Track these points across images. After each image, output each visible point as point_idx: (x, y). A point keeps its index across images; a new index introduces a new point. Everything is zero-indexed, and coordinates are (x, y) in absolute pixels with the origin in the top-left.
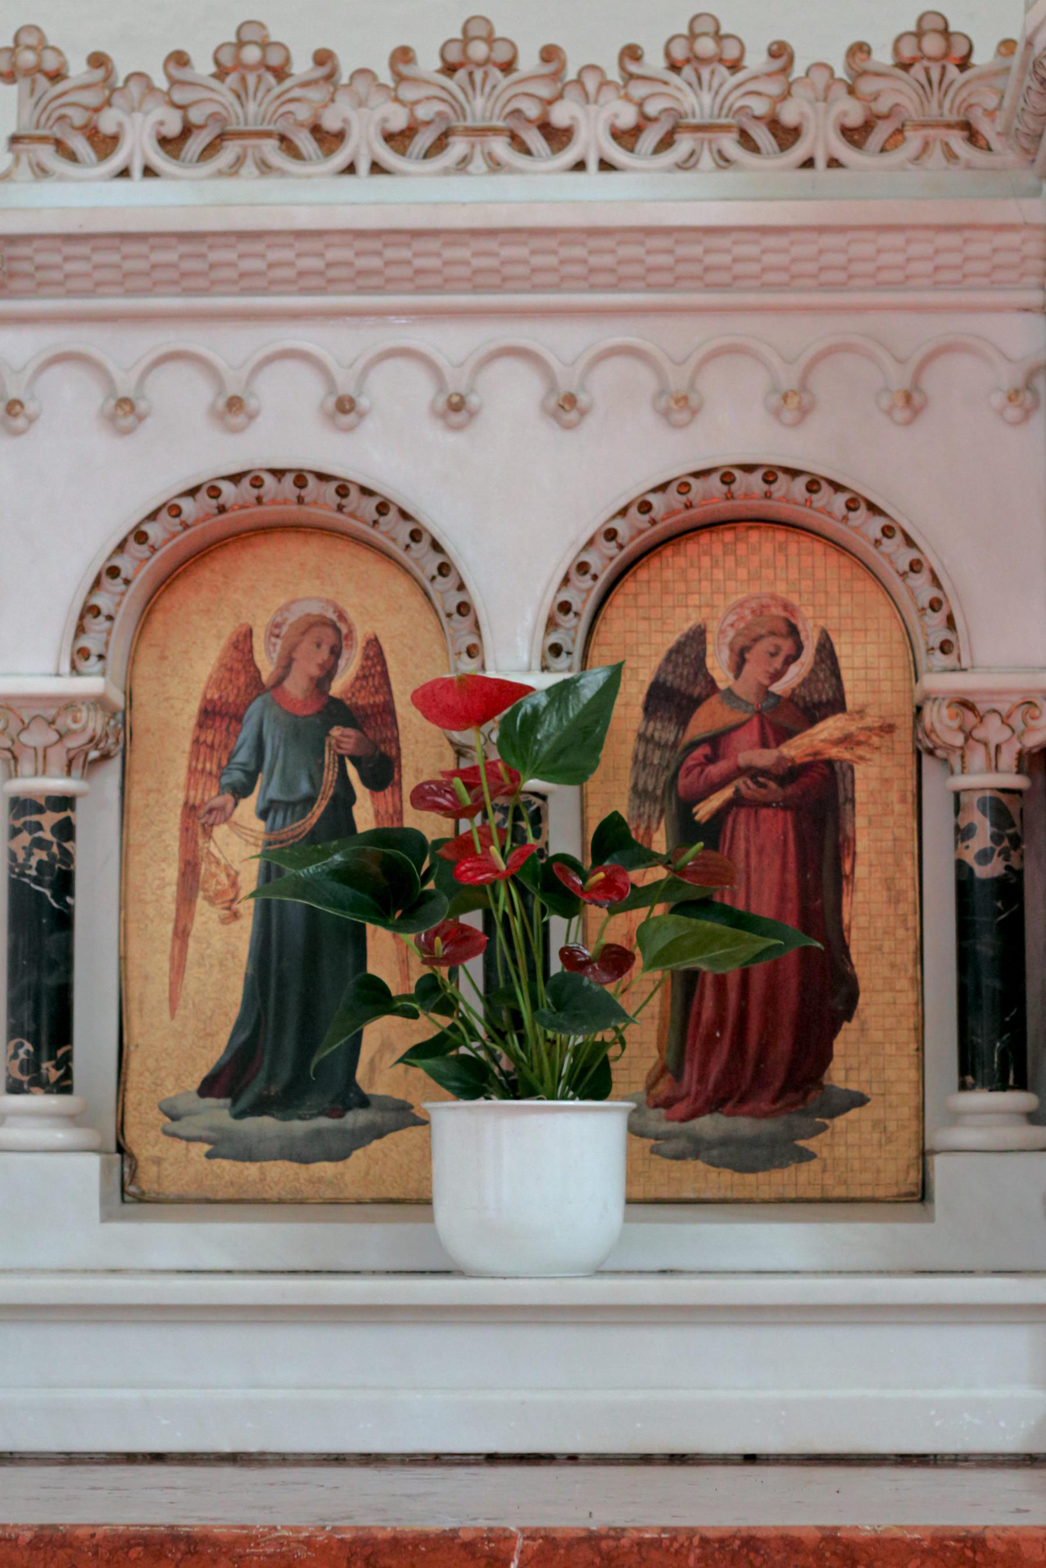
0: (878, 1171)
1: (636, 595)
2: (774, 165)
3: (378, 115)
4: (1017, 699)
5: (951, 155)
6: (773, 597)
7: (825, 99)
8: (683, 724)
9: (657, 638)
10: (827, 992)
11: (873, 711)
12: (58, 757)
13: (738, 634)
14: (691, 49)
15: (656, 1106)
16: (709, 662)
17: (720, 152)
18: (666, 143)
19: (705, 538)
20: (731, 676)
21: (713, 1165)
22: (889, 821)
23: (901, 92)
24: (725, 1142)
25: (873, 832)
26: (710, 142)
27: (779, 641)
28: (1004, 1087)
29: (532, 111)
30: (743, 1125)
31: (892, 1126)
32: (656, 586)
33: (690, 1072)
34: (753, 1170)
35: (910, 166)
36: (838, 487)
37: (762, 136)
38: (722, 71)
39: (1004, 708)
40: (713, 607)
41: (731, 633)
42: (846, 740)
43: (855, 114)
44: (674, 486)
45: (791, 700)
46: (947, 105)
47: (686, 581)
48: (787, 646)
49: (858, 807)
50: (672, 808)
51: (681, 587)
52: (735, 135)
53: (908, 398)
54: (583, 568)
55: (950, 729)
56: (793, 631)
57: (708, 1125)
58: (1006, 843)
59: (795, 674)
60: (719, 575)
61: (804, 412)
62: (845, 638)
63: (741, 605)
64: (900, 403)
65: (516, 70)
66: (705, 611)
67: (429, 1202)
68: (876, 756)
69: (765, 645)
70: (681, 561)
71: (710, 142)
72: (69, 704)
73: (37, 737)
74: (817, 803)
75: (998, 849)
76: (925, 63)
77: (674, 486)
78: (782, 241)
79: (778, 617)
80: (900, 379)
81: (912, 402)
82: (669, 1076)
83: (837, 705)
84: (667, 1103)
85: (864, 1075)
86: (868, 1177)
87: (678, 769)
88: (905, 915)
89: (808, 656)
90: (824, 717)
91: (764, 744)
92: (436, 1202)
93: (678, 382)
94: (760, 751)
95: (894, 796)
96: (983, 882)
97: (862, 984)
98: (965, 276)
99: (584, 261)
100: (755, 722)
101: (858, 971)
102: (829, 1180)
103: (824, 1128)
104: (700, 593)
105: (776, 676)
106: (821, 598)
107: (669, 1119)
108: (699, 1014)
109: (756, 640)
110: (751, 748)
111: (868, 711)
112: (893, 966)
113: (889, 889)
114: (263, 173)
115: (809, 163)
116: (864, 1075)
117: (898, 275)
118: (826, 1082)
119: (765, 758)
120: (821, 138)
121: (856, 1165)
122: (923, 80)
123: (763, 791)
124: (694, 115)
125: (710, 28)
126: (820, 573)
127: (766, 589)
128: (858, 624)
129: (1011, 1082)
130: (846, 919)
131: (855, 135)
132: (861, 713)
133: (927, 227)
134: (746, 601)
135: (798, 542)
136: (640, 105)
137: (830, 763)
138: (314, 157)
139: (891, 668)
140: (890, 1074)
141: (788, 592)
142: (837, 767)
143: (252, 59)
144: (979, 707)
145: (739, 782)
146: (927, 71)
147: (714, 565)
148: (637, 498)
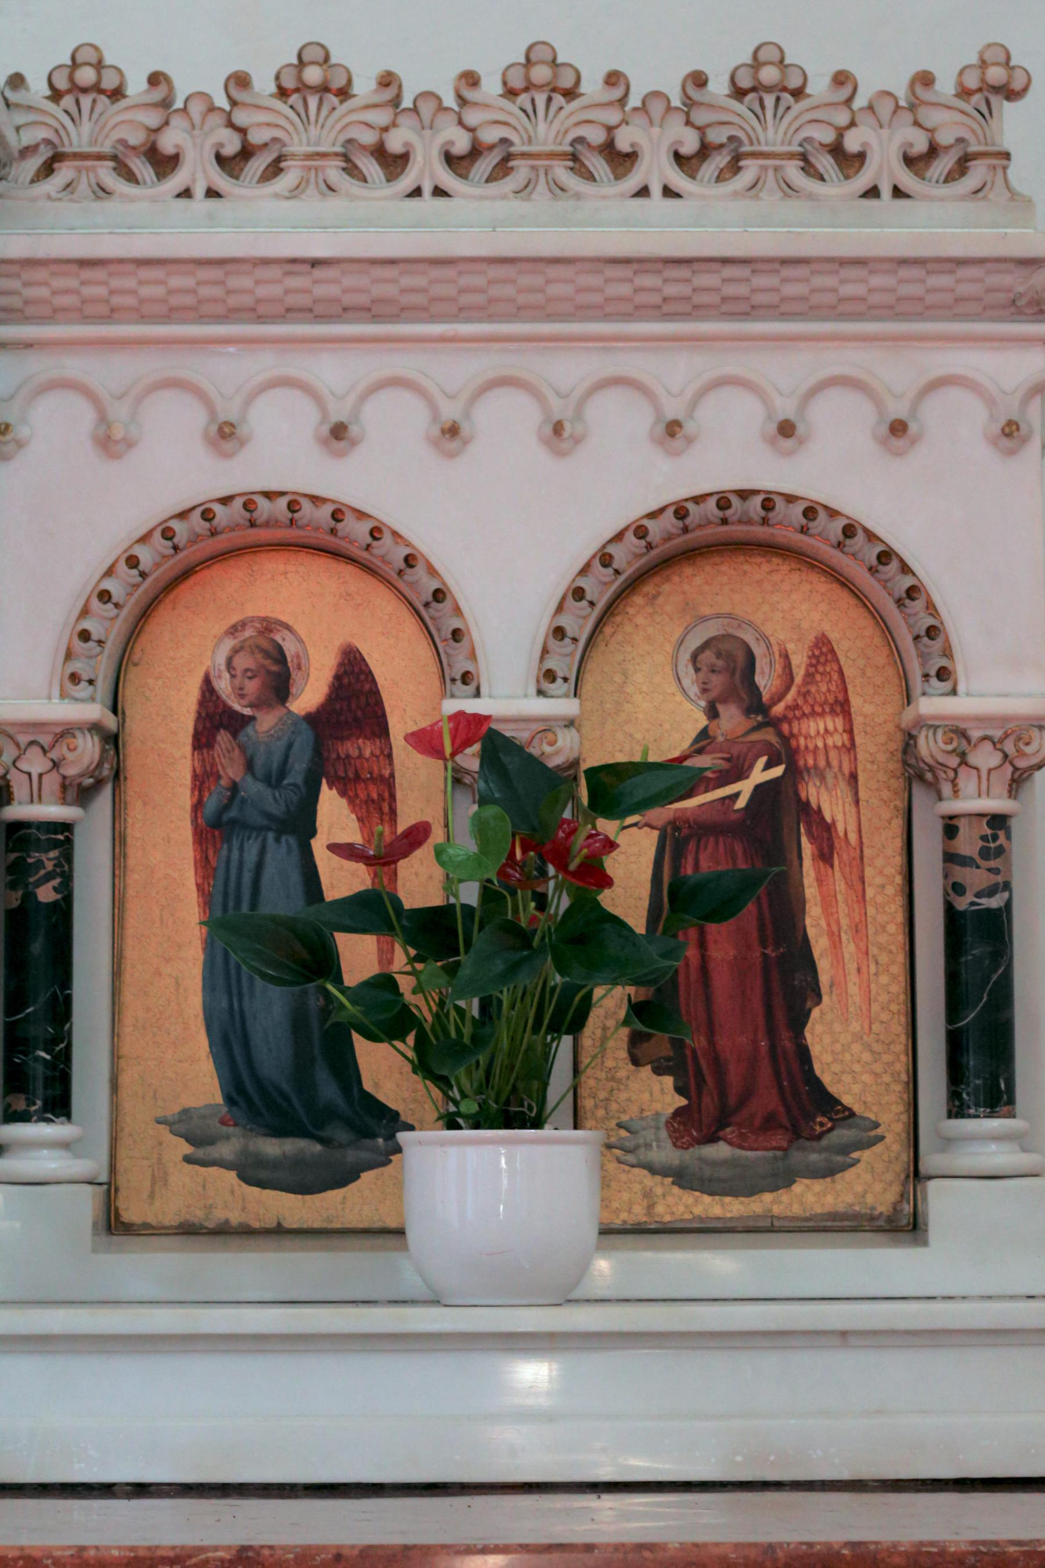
2: (838, 189)
3: (212, 140)
12: (52, 783)
29: (368, 138)
54: (578, 593)
65: (124, 96)
67: (400, 1232)
72: (66, 732)
73: (35, 763)
92: (407, 1231)
99: (77, 292)
114: (786, 195)
138: (149, 182)
143: (770, 82)
148: (634, 522)
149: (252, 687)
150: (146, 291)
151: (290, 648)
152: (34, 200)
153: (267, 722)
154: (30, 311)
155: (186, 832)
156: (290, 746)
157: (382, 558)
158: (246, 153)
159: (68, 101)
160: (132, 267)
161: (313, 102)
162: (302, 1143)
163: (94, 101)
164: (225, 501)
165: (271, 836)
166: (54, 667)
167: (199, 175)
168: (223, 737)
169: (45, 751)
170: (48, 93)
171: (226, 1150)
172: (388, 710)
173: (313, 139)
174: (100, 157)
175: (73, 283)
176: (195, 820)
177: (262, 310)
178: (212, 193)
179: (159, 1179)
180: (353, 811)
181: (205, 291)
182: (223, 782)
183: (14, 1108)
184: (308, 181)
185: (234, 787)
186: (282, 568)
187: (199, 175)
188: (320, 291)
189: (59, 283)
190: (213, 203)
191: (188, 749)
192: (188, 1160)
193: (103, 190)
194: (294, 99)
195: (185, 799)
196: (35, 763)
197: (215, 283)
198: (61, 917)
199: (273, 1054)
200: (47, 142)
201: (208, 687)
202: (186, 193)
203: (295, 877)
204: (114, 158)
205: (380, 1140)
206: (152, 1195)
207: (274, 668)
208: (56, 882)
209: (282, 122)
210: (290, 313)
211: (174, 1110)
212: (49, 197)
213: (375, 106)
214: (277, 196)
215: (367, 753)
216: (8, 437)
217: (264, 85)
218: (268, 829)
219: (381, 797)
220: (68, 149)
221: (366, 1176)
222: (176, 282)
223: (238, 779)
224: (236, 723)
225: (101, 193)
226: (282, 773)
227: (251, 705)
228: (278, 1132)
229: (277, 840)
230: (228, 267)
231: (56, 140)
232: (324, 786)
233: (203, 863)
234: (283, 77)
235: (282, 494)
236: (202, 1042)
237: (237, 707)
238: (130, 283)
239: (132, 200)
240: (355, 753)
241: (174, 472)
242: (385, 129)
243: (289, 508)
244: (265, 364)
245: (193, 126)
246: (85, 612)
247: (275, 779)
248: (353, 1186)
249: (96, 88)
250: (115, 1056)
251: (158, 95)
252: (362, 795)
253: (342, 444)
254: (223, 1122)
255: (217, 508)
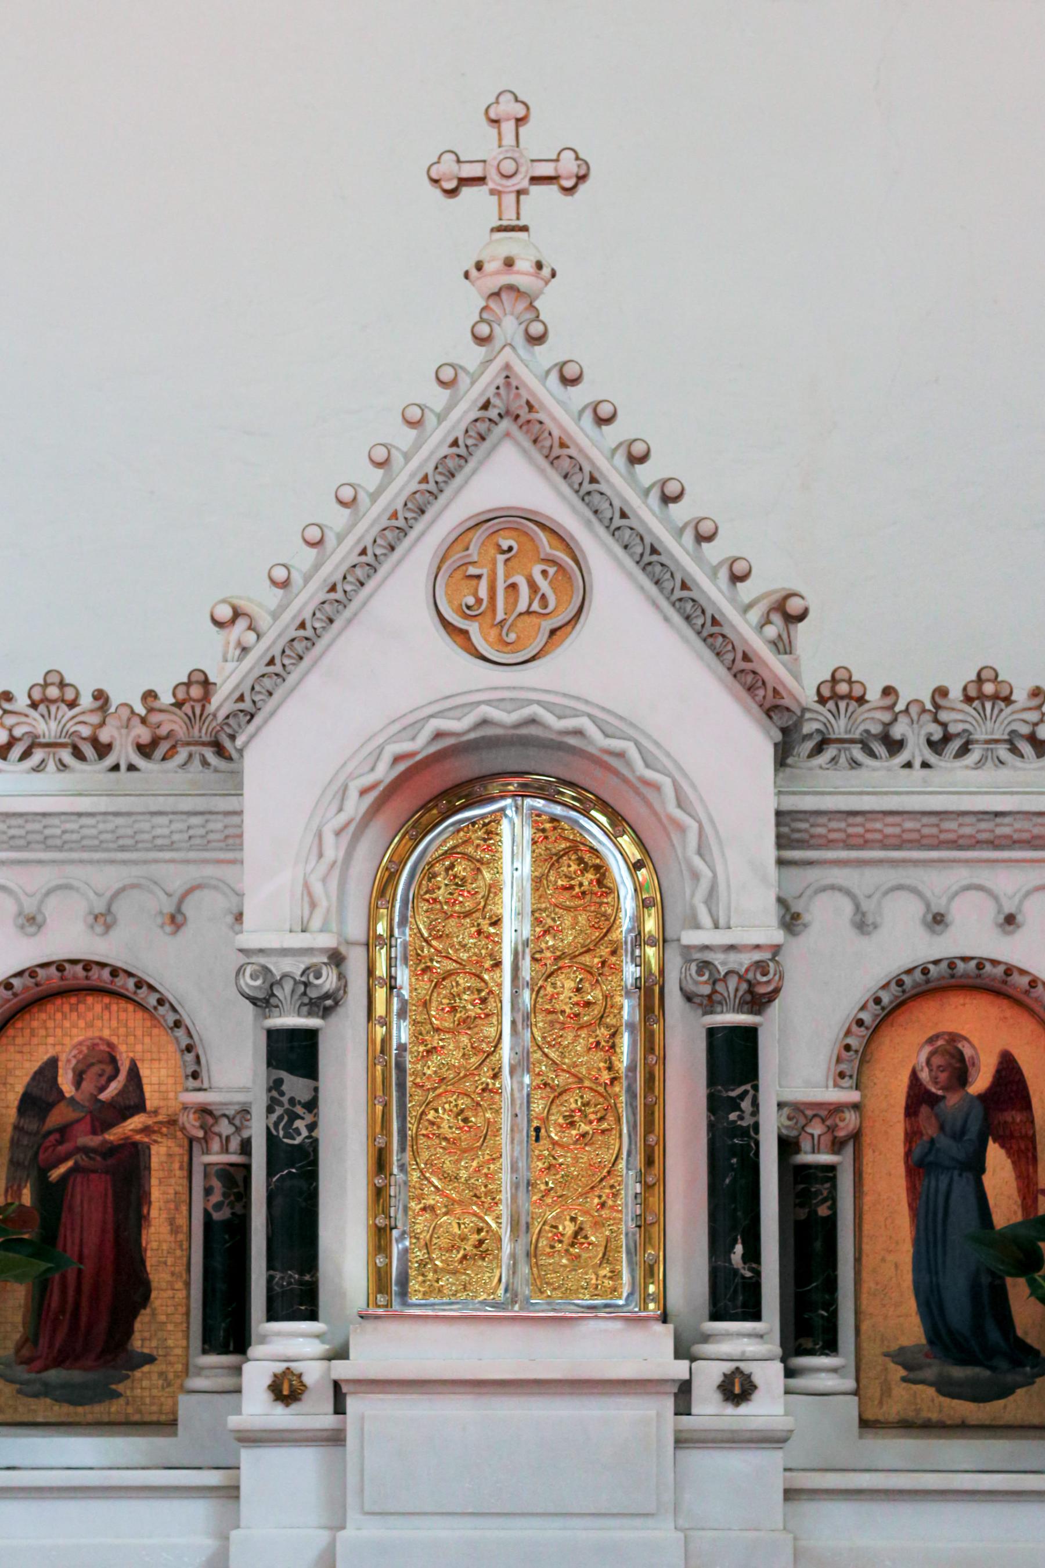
0: (162, 1405)
1: (14, 1037)
4: (237, 1107)
5: (205, 763)
6: (101, 1038)
7: (127, 727)
8: (43, 1120)
9: (27, 1065)
10: (130, 1288)
11: (163, 1111)
12: (826, 1140)
13: (78, 1062)
14: (44, 693)
15: (22, 1363)
16: (60, 1080)
17: (60, 760)
18: (26, 755)
19: (58, 1001)
20: (73, 1089)
21: (56, 1400)
22: (173, 1181)
23: (175, 722)
24: (64, 1386)
25: (162, 1190)
26: (54, 754)
27: (103, 1066)
28: (226, 1352)
29: (1025, 730)
30: (76, 1376)
31: (171, 1376)
32: (27, 1032)
33: (43, 1341)
34: (81, 1404)
35: (180, 770)
36: (130, 974)
37: (88, 750)
38: (64, 707)
39: (231, 1112)
40: (63, 1045)
41: (74, 1062)
42: (146, 1130)
43: (144, 735)
44: (27, 974)
45: (111, 1104)
46: (204, 731)
47: (46, 1029)
48: (109, 1070)
49: (153, 1173)
50: (34, 1173)
51: (42, 1032)
52: (70, 750)
53: (173, 918)
55: (193, 1126)
56: (113, 1060)
57: (53, 1375)
58: (232, 1198)
59: (114, 1087)
60: (67, 1024)
61: (108, 927)
62: (146, 1065)
63: (80, 1044)
64: (168, 920)
66: (58, 1048)
67: (239, 1468)
68: (164, 1140)
69: (95, 1069)
70: (43, 1016)
71: (54, 754)
72: (837, 1109)
74: (128, 1168)
75: (227, 1202)
76: (192, 703)
77: (27, 974)
78: (90, 821)
79: (103, 1051)
80: (169, 907)
81: (176, 921)
82: (29, 1344)
83: (140, 1107)
84: (27, 1361)
85: (154, 1344)
86: (154, 1408)
87: (39, 1148)
88: (181, 1241)
89: (122, 1077)
90: (132, 1115)
91: (94, 1132)
93: (30, 906)
94: (91, 1137)
95: (177, 1165)
96: (217, 1222)
97: (154, 1285)
98: (209, 842)
100: (88, 1117)
101: (151, 1277)
102: (130, 1410)
103: (127, 1377)
104: (55, 1036)
105: (102, 1089)
106: (131, 1039)
107: (30, 1371)
108: (49, 1305)
109: (91, 1065)
110: (86, 1135)
111: (160, 1111)
112: (173, 1274)
113: (171, 1224)
115: (116, 768)
116: (154, 1344)
117: (167, 842)
118: (129, 1348)
119: (93, 1141)
120: (124, 752)
121: (148, 1400)
122: (190, 714)
123: (92, 1162)
124: (44, 736)
125: (57, 680)
126: (131, 1024)
127: (97, 1034)
128: (155, 1056)
129: (231, 1348)
130: (144, 1245)
131: (145, 750)
132: (156, 1112)
133: (182, 813)
134: (84, 1041)
135: (118, 1003)
136: (10, 730)
137: (135, 1145)
139: (175, 1084)
140: (170, 1343)
141: (111, 1035)
142: (140, 1146)
144: (215, 1112)
145: (78, 1157)
146: (193, 708)
147: (64, 1017)
149: (943, 1076)
150: (889, 830)
151: (968, 1052)
152: (811, 769)
153: (953, 1100)
154: (812, 842)
155: (901, 1170)
156: (968, 1115)
157: (1036, 999)
158: (947, 738)
159: (831, 705)
160: (880, 816)
161: (988, 705)
162: (977, 1370)
163: (848, 705)
164: (936, 962)
165: (956, 1173)
166: (829, 1068)
167: (917, 753)
168: (924, 1110)
169: (823, 1121)
170: (816, 699)
171: (930, 1373)
172: (1031, 1093)
173: (989, 730)
174: (852, 741)
175: (842, 825)
176: (906, 1162)
177: (961, 842)
178: (925, 765)
179: (886, 1391)
180: (1009, 1157)
181: (926, 831)
182: (925, 1138)
183: (804, 1346)
184: (987, 758)
185: (932, 1141)
186: (962, 1001)
187: (917, 753)
188: (999, 831)
189: (834, 825)
190: (926, 772)
191: (902, 1117)
192: (904, 1379)
193: (855, 762)
194: (976, 703)
195: (900, 1149)
196: (816, 1129)
197: (933, 825)
198: (831, 1224)
199: (958, 1313)
200: (818, 731)
201: (914, 1076)
202: (908, 765)
203: (972, 1199)
204: (861, 742)
205: (1028, 1369)
206: (881, 1403)
207: (958, 1065)
208: (829, 1203)
209: (970, 719)
210: (977, 844)
211: (894, 1347)
212: (821, 767)
213: (1030, 709)
214: (967, 767)
215: (1018, 1120)
216: (799, 922)
217: (956, 694)
218: (954, 1168)
219: (1027, 1149)
220: (832, 736)
221: (1020, 1392)
222: (909, 825)
223: (935, 1136)
224: (933, 1100)
225: (854, 765)
226: (963, 1131)
227: (941, 1089)
228: (963, 1362)
229: (960, 1175)
230: (942, 816)
231: (825, 730)
232: (990, 1142)
233: (912, 1190)
234: (969, 689)
235: (972, 958)
236: (911, 1305)
237: (933, 1090)
238: (878, 825)
239: (874, 769)
240: (1009, 1119)
241: (904, 945)
242: (1036, 724)
243: (1030, 983)
244: (962, 875)
245: (912, 721)
246: (848, 1033)
247: (958, 1136)
248: (1011, 1398)
249: (849, 697)
250: (857, 1312)
251: (888, 701)
252: (1015, 1147)
253: (1011, 928)
254: (927, 1356)
255: (931, 967)
